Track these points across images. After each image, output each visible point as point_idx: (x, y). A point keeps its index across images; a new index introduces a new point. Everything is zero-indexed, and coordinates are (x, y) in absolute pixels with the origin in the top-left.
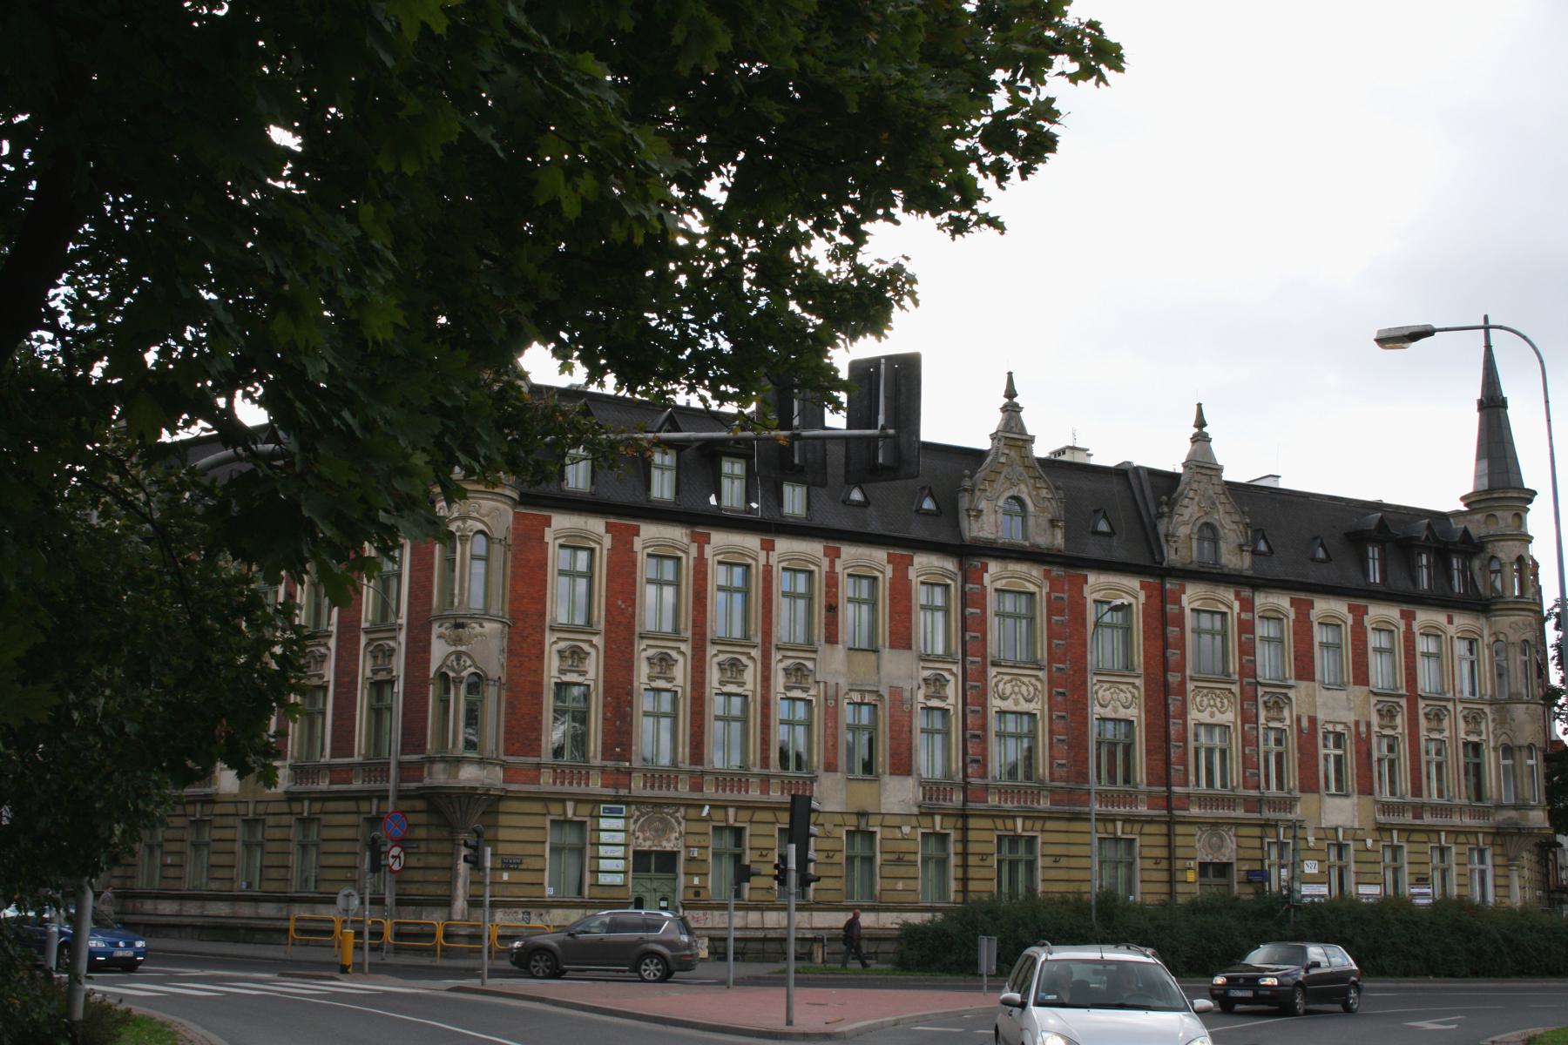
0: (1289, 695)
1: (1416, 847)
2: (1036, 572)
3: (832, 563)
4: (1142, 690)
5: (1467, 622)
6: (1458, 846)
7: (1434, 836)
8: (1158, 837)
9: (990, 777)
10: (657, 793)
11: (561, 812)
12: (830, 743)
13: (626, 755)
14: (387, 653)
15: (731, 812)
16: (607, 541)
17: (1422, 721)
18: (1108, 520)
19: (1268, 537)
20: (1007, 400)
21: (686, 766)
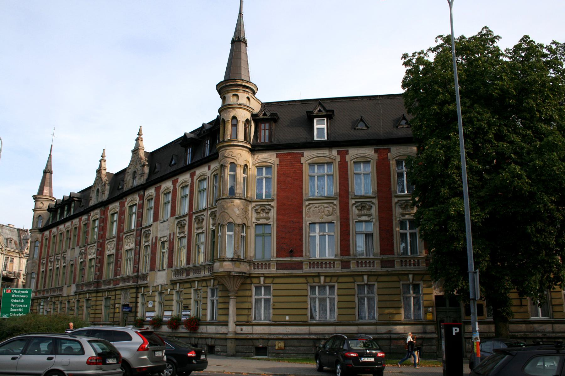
6: (340, 284)
7: (359, 278)
9: (396, 254)
11: (318, 281)
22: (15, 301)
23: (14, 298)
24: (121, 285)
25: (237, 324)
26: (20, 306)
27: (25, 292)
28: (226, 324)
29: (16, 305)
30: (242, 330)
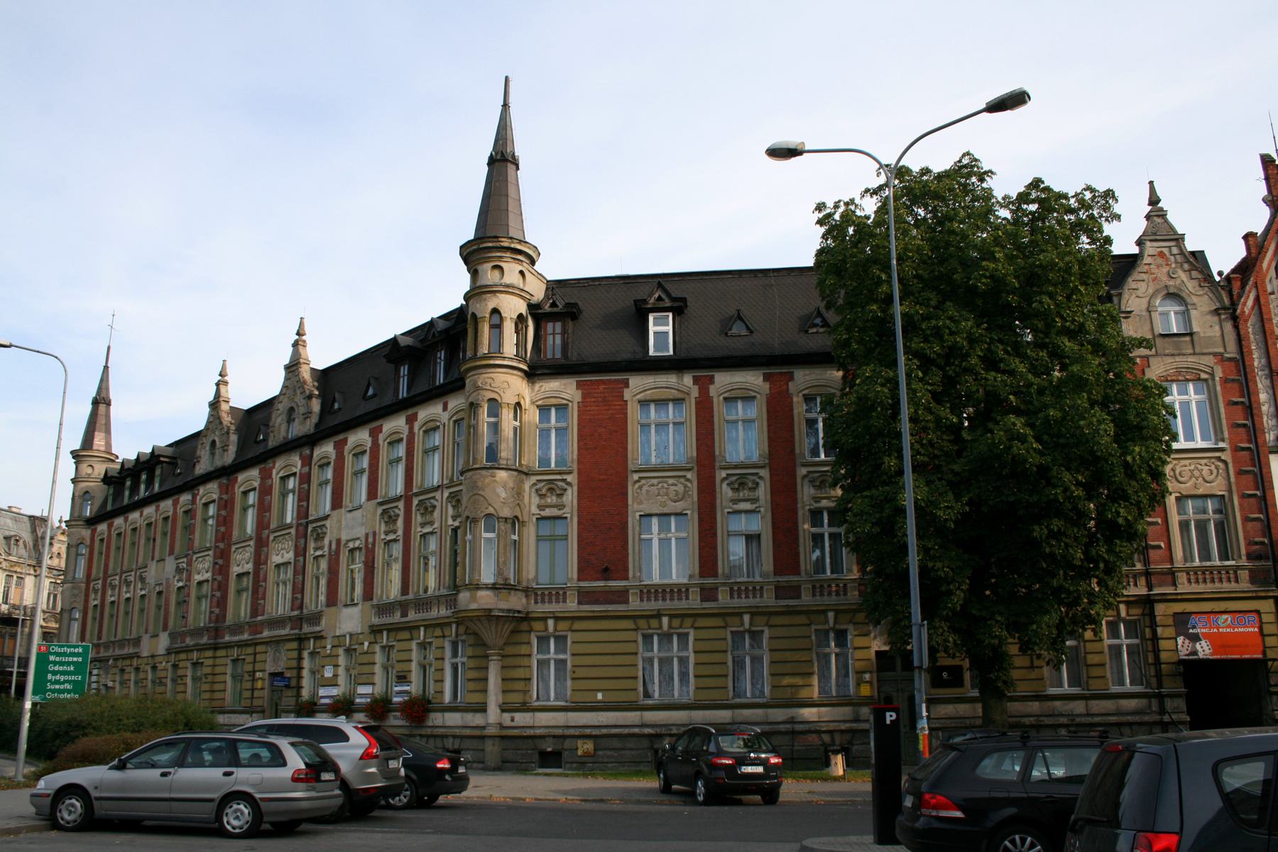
1: (704, 634)
4: (695, 483)
5: (459, 402)
6: (573, 633)
9: (803, 573)
12: (501, 560)
13: (714, 574)
14: (430, 509)
15: (551, 623)
16: (766, 387)
17: (401, 513)
18: (1257, 290)
19: (1259, 287)
22: (57, 668)
23: (55, 663)
24: (266, 633)
25: (504, 708)
26: (66, 678)
27: (76, 650)
28: (482, 708)
29: (58, 677)
30: (513, 720)
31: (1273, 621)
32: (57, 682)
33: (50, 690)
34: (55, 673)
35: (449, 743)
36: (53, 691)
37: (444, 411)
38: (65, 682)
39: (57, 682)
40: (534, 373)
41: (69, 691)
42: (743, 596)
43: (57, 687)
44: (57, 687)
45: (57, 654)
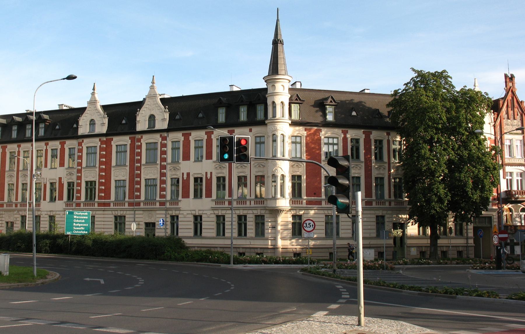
0: (96, 170)
2: (301, 128)
3: (19, 149)
8: (132, 215)
10: (147, 207)
20: (152, 84)
21: (14, 201)
22: (77, 221)
23: (76, 219)
26: (82, 225)
27: (85, 214)
29: (78, 225)
31: (97, 231)
32: (78, 227)
33: (75, 230)
34: (76, 223)
35: (259, 251)
36: (76, 230)
37: (250, 132)
38: (81, 227)
39: (78, 227)
40: (294, 124)
41: (83, 230)
42: (382, 204)
43: (78, 228)
44: (78, 228)
45: (77, 215)
